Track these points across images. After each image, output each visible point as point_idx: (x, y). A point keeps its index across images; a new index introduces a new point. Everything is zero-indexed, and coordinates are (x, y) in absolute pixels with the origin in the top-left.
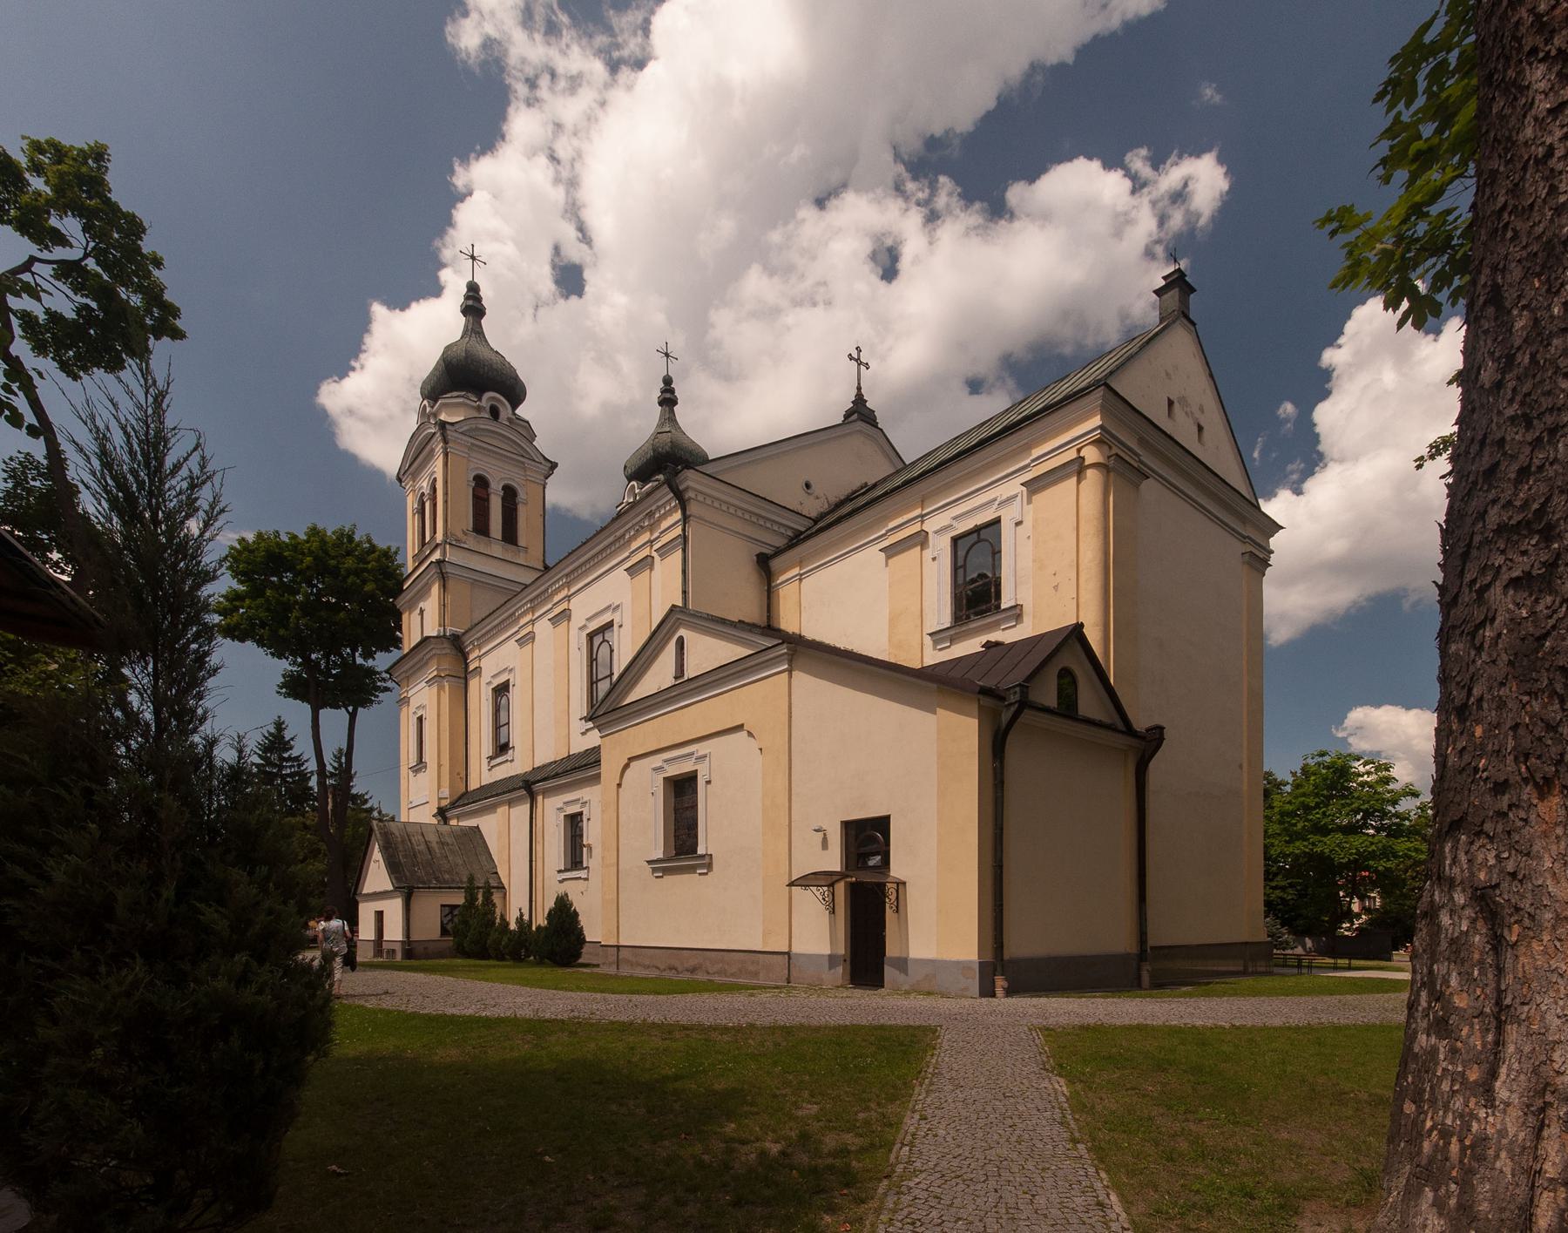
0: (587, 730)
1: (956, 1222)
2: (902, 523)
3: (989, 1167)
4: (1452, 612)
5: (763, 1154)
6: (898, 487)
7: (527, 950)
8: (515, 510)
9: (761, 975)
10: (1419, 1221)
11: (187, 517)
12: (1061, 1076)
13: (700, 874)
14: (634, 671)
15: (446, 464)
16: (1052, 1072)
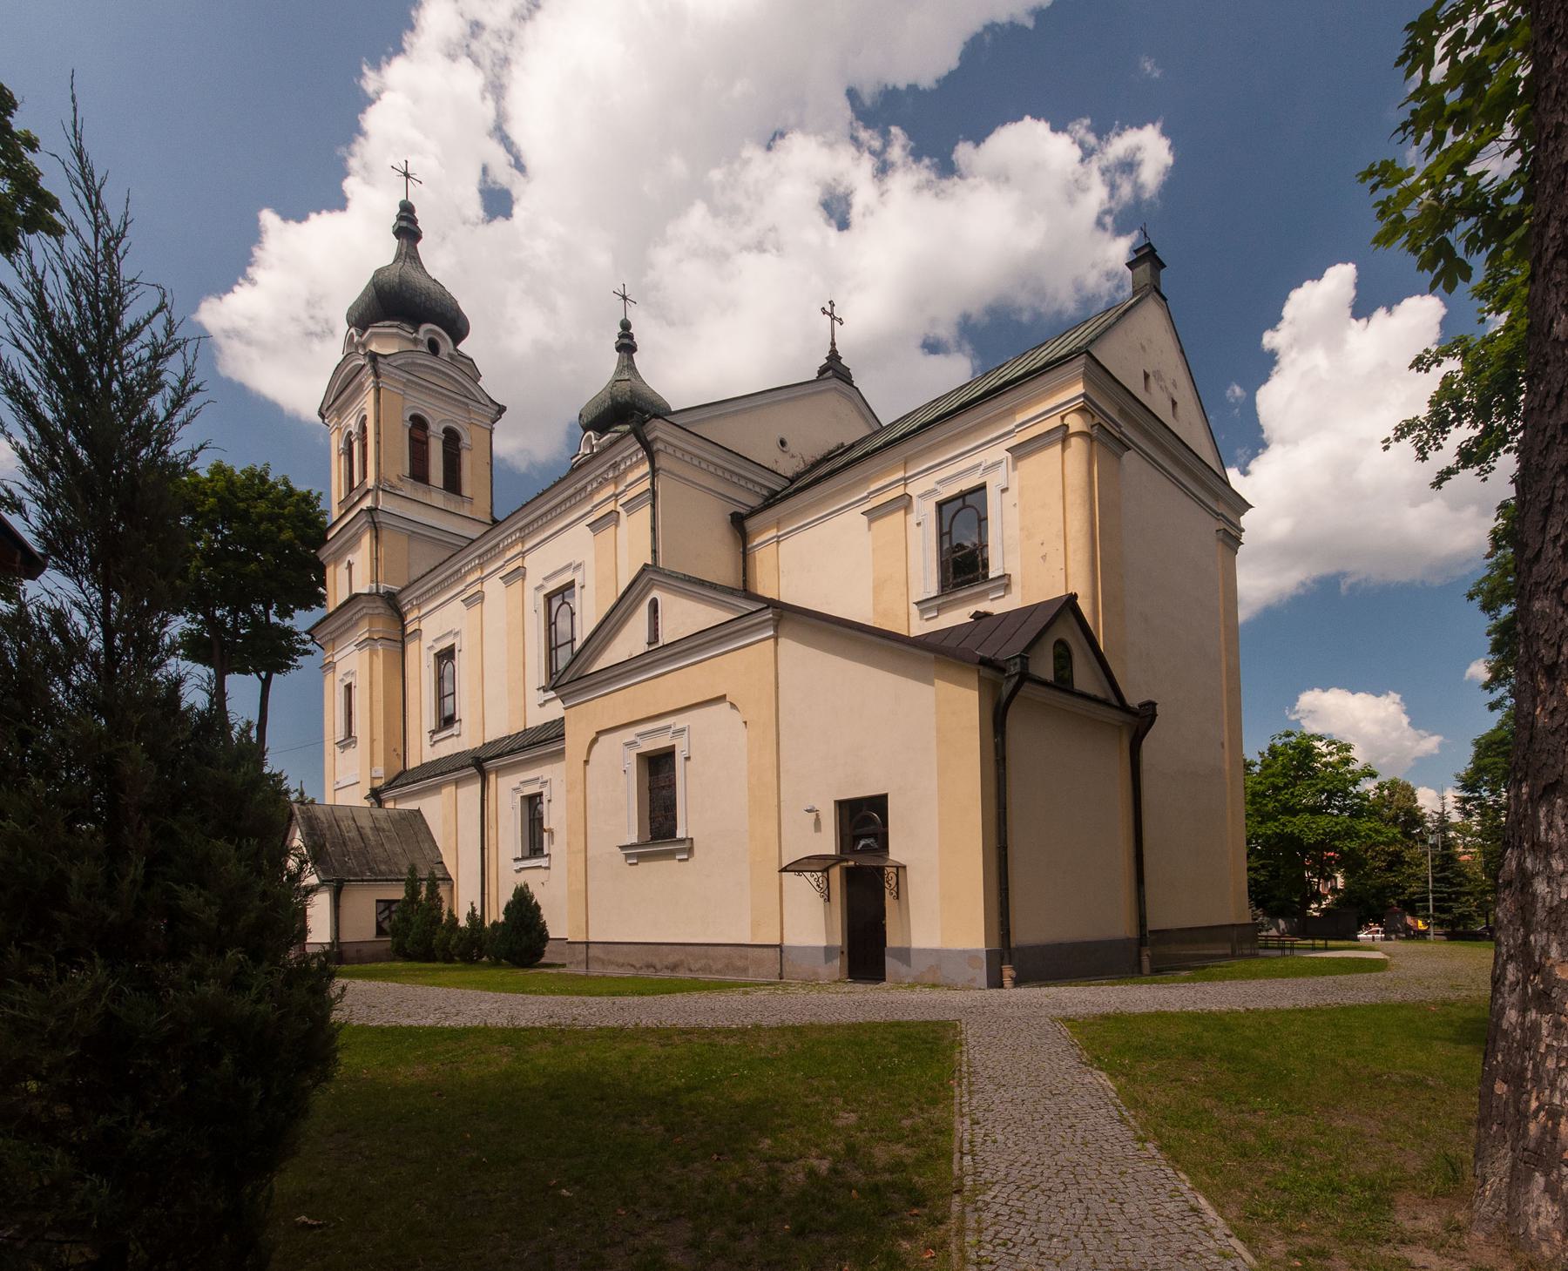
0: (546, 701)
1: (1050, 1239)
2: (883, 483)
3: (1064, 1174)
4: (1534, 570)
5: (812, 1173)
6: (896, 440)
7: (480, 949)
8: (459, 456)
9: (751, 971)
10: (1531, 1209)
11: (152, 393)
12: (1101, 1070)
13: (680, 860)
14: (602, 634)
15: (377, 400)
16: (1091, 1065)
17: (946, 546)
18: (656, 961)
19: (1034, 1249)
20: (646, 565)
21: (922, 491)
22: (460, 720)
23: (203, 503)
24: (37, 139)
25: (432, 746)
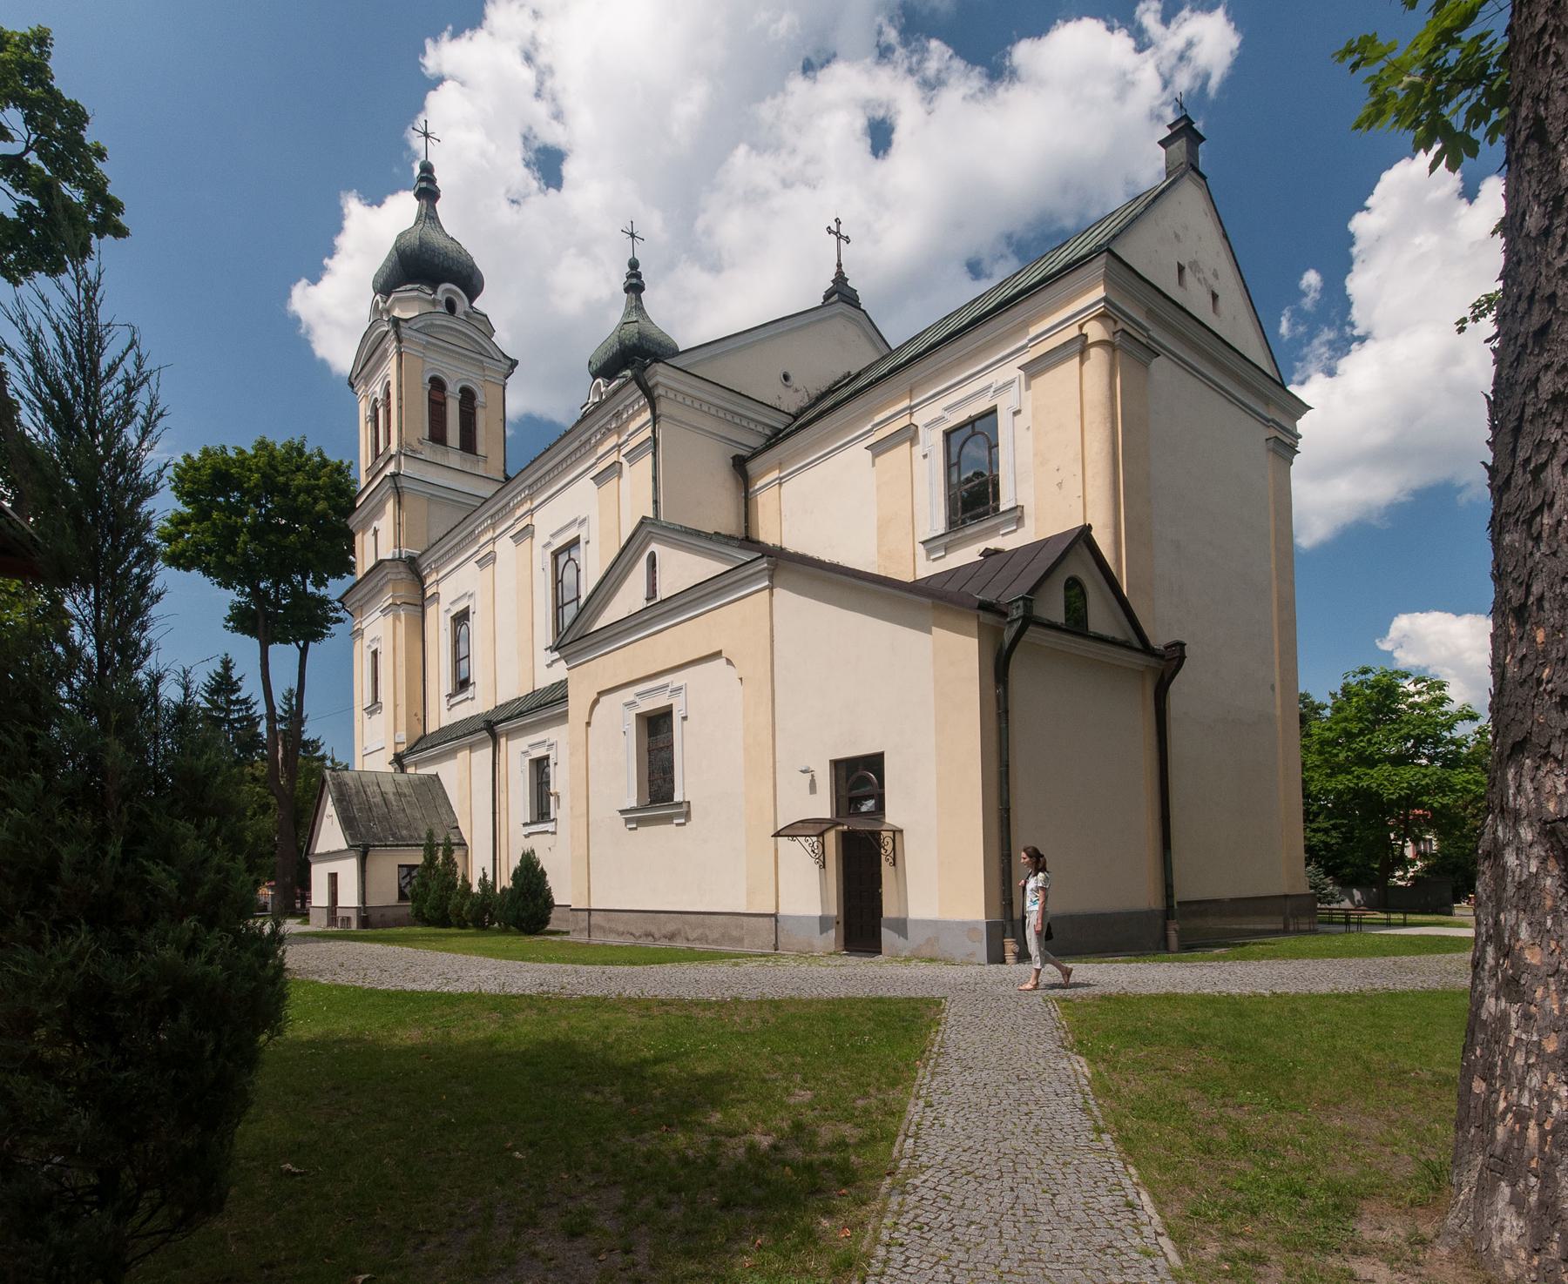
1: (968, 1226)
2: (888, 415)
3: (1003, 1162)
5: (752, 1148)
6: (902, 365)
7: (491, 915)
9: (746, 941)
10: (1495, 1222)
11: (126, 423)
12: (1082, 1055)
13: (678, 825)
16: (1071, 1050)
17: (954, 478)
18: (653, 929)
19: (949, 1234)
20: (644, 518)
21: (928, 420)
23: (249, 479)
24: (105, 149)
25: (449, 710)
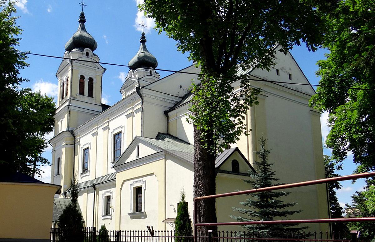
15: (72, 73)
22: (89, 171)
25: (81, 178)
